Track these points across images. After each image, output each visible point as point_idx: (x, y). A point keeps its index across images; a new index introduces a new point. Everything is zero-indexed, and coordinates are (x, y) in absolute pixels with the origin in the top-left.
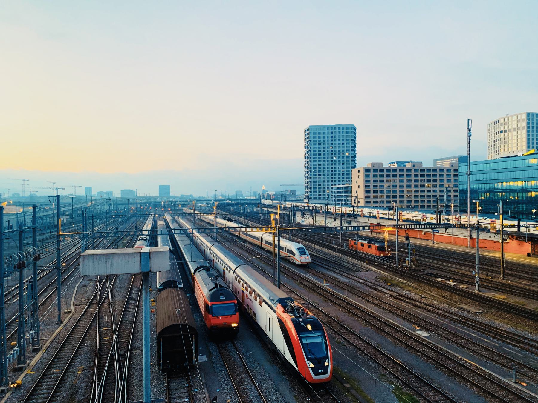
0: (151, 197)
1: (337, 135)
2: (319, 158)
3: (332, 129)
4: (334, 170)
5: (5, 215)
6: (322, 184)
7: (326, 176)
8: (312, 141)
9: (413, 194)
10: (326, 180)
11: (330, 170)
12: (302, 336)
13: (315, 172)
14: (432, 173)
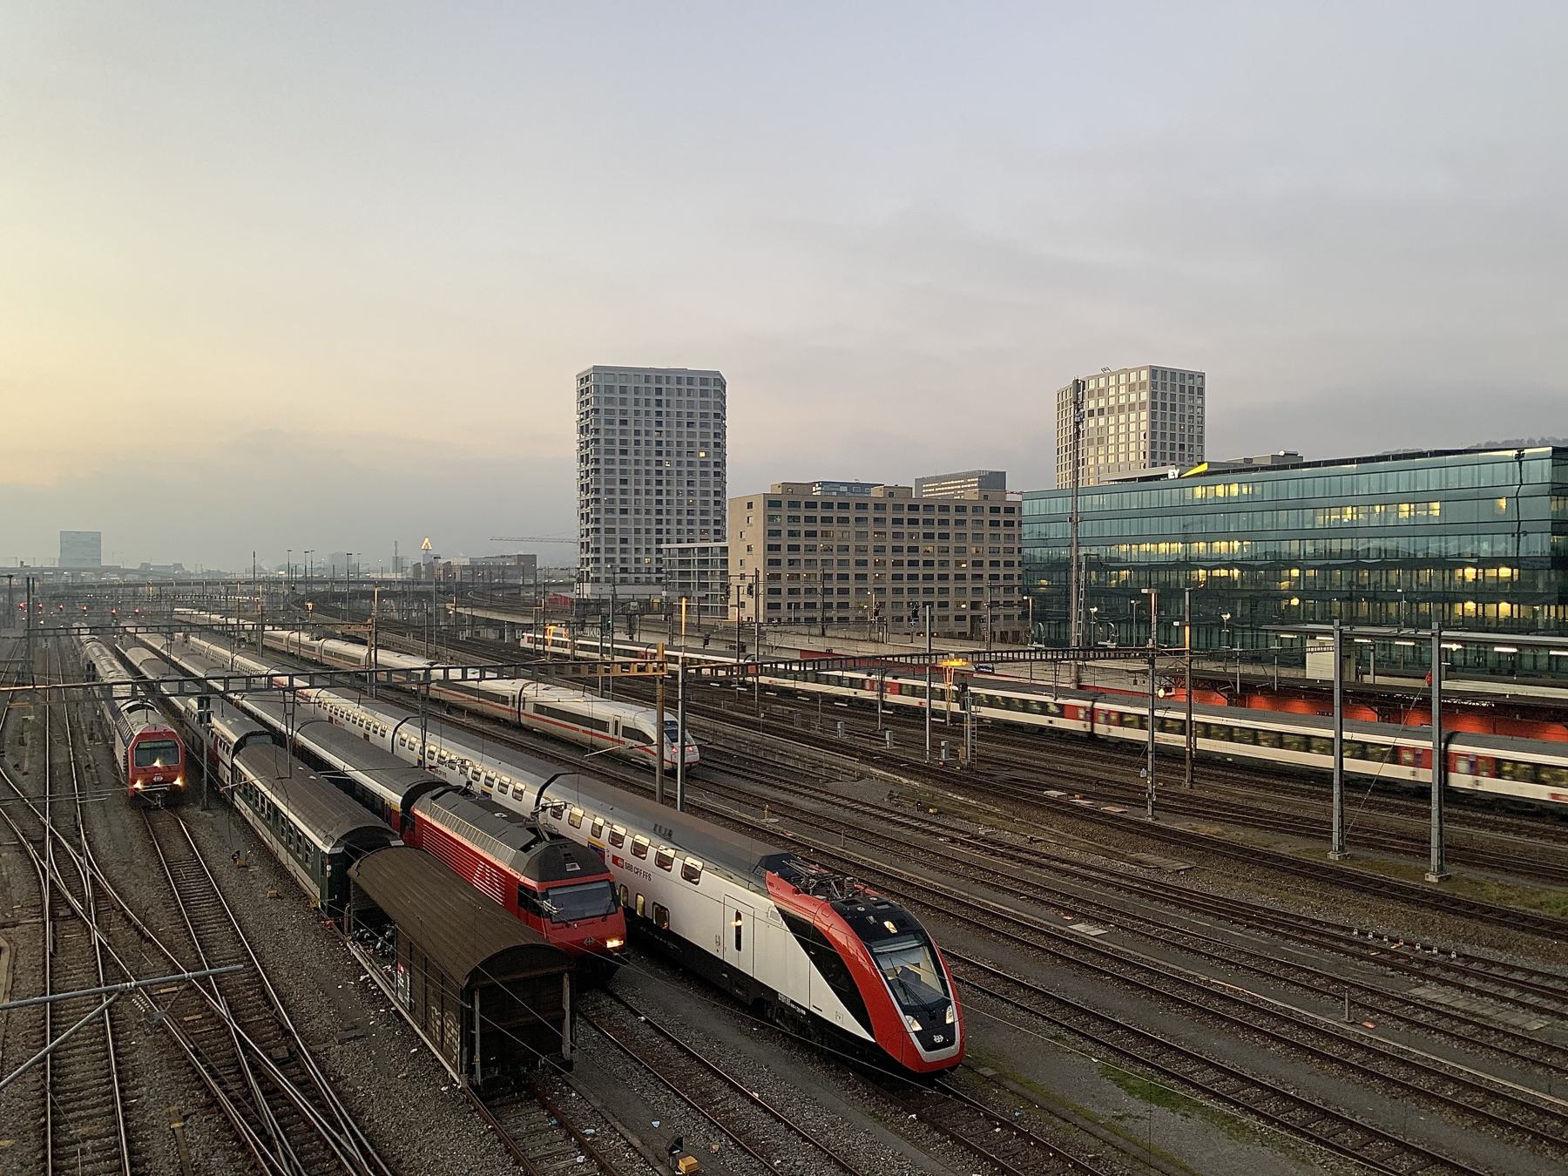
0: (36, 569)
1: (674, 399)
3: (658, 380)
4: (664, 498)
6: (632, 537)
7: (643, 516)
8: (602, 412)
9: (890, 571)
10: (643, 527)
12: (875, 950)
13: (612, 501)
14: (936, 516)
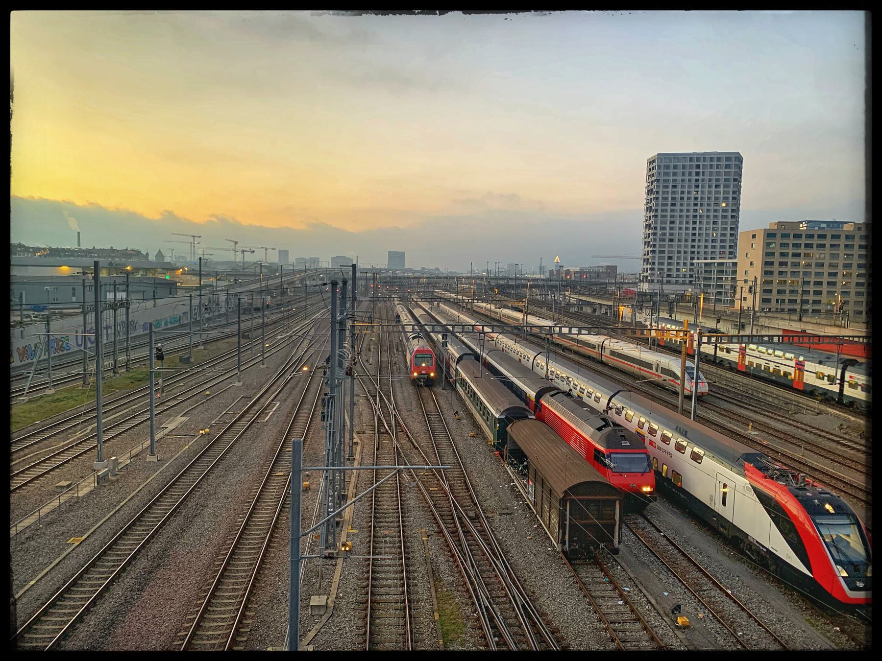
0: (378, 269)
2: (672, 211)
3: (698, 159)
5: (359, 280)
7: (683, 243)
10: (682, 250)
11: (691, 232)
